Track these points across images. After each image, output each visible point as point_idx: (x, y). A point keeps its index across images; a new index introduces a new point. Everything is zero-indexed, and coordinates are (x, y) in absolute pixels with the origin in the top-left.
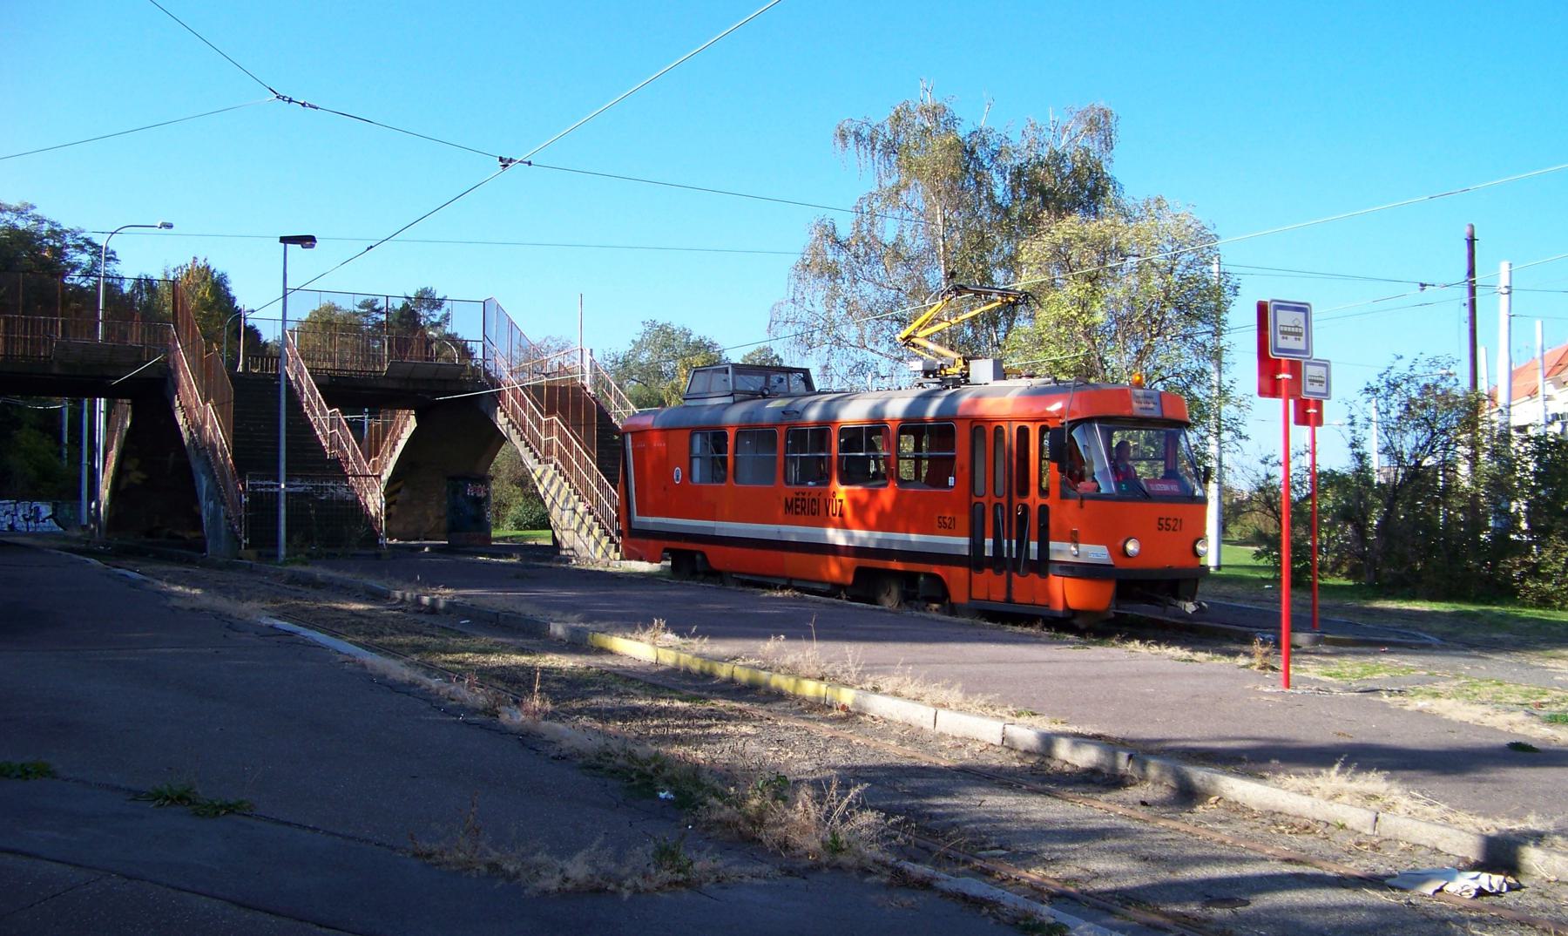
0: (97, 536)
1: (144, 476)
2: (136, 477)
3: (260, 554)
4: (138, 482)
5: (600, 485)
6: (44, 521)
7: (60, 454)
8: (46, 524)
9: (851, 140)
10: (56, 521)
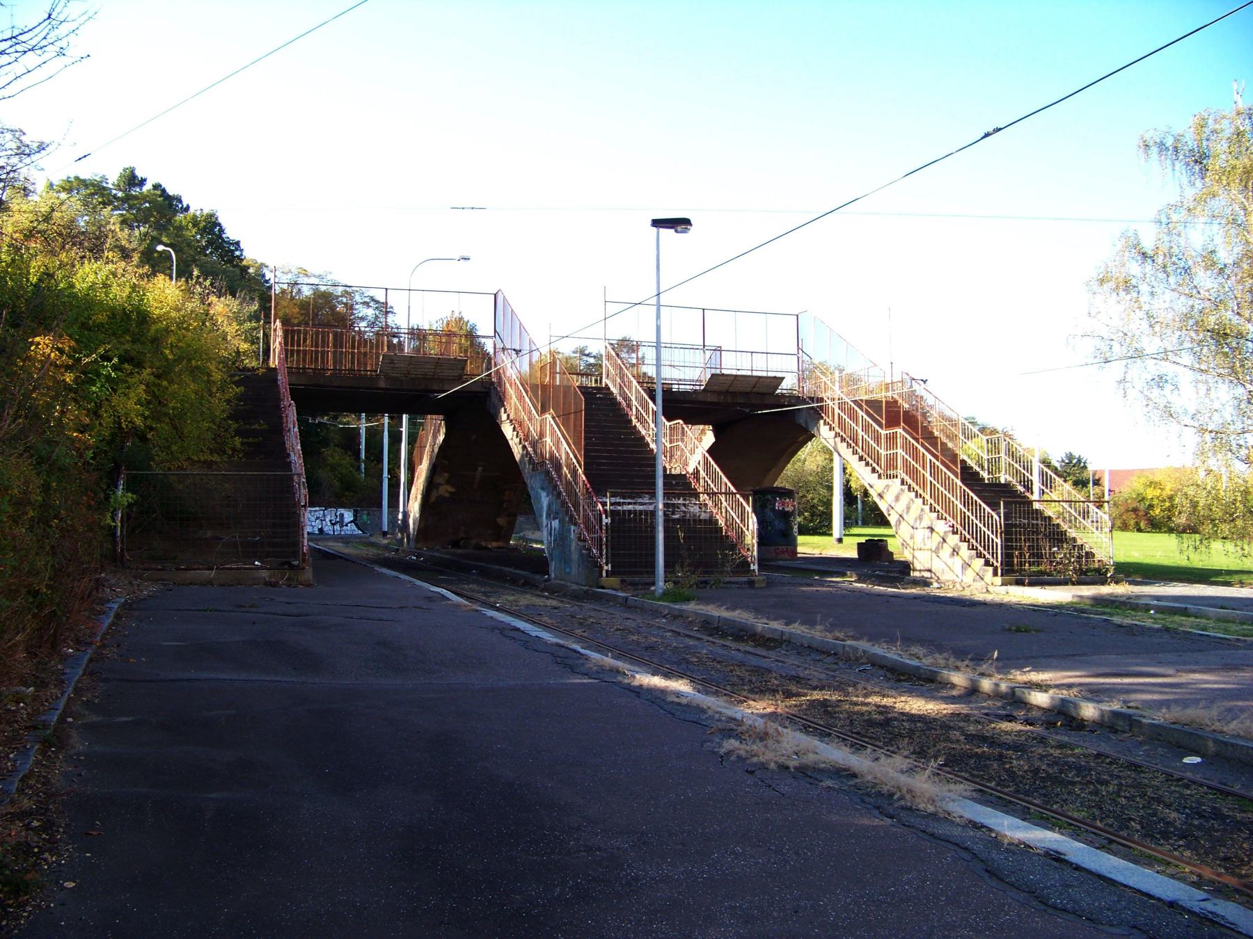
0: (405, 545)
1: (452, 490)
2: (445, 490)
3: (622, 581)
4: (447, 495)
5: (966, 502)
6: (346, 525)
7: (359, 468)
8: (348, 528)
9: (1155, 150)
10: (356, 525)
